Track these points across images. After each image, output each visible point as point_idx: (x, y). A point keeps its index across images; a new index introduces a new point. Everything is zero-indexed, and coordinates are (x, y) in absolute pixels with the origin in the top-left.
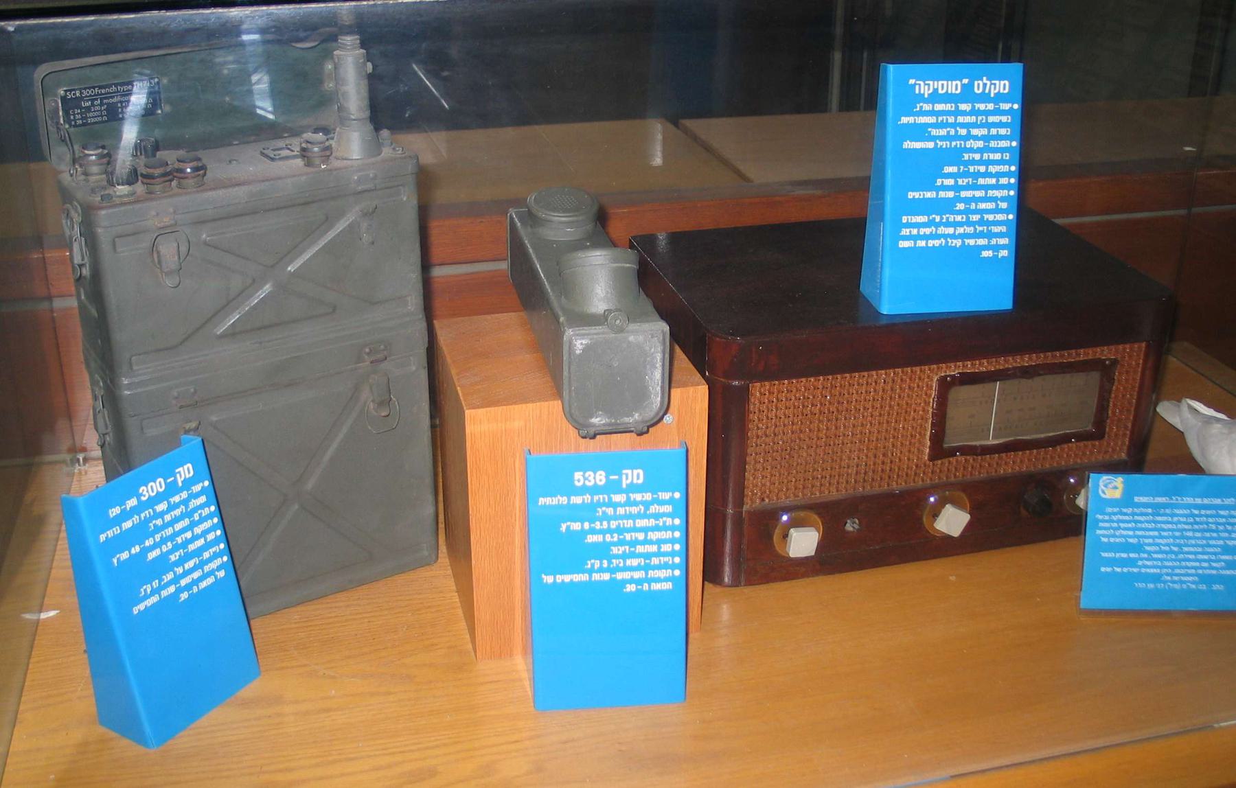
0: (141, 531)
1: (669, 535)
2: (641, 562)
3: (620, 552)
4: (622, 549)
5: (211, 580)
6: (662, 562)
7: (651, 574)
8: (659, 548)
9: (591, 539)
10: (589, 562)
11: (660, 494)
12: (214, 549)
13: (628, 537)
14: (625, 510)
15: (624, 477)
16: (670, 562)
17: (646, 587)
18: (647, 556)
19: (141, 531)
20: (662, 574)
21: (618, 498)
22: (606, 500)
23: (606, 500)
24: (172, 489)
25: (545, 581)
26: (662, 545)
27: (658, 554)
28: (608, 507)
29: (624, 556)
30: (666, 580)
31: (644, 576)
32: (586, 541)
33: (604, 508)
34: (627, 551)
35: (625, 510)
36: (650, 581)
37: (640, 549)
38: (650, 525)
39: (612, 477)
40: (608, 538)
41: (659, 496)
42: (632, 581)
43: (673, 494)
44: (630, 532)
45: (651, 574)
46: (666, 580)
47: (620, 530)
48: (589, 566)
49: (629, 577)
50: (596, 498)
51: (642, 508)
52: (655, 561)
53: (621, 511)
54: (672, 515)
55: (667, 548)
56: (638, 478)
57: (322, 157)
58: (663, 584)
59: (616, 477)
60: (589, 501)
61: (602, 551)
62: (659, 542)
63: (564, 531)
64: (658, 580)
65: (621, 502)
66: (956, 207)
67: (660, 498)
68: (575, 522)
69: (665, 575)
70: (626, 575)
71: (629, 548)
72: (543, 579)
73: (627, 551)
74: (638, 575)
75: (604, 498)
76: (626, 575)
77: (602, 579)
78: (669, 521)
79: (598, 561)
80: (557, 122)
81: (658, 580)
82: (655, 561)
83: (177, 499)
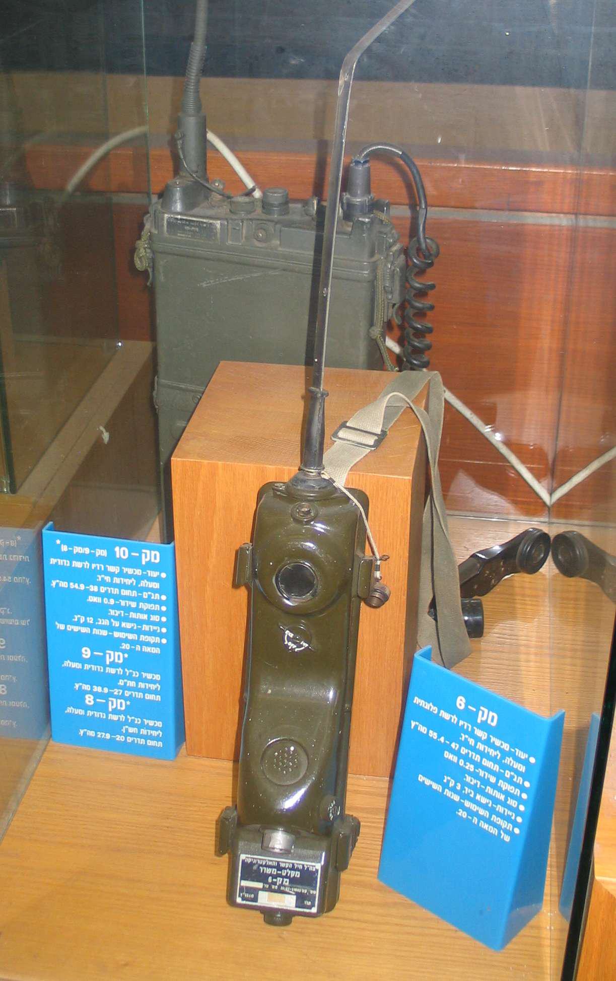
0: (88, 577)
1: (157, 607)
2: (134, 626)
3: (117, 615)
4: (118, 613)
5: (494, 831)
6: (152, 630)
7: (143, 638)
8: (149, 617)
9: (92, 599)
10: (76, 616)
11: (149, 571)
12: (155, 628)
13: (123, 603)
14: (121, 581)
15: (143, 555)
16: (159, 631)
17: (138, 648)
18: (140, 622)
19: (88, 577)
20: (152, 639)
21: (111, 569)
22: (103, 569)
23: (103, 569)
24: (134, 562)
25: (58, 628)
26: (152, 616)
27: (149, 622)
28: (106, 575)
29: (119, 618)
30: (155, 645)
31: (136, 639)
32: (88, 600)
33: (103, 576)
34: (123, 615)
35: (121, 581)
36: (143, 644)
37: (133, 615)
38: (133, 595)
39: (133, 554)
40: (106, 601)
41: (147, 573)
42: (126, 640)
43: (160, 574)
44: (125, 600)
45: (143, 638)
46: (155, 645)
47: (117, 597)
48: (76, 620)
49: (124, 637)
50: (94, 566)
51: (135, 581)
52: (146, 627)
53: (117, 580)
54: (159, 591)
55: (155, 618)
56: (155, 558)
57: (521, 682)
58: (153, 648)
59: (137, 555)
60: (88, 567)
61: (100, 611)
62: (149, 612)
63: (54, 587)
64: (148, 644)
65: (115, 572)
66: (458, 812)
67: (149, 575)
68: (63, 581)
69: (154, 641)
70: (122, 635)
71: (124, 613)
72: (57, 626)
73: (123, 615)
74: (131, 636)
75: (100, 567)
76: (122, 635)
77: (101, 634)
78: (157, 596)
79: (84, 617)
80: (599, 809)
81: (148, 644)
82: (146, 627)
83: (130, 571)
